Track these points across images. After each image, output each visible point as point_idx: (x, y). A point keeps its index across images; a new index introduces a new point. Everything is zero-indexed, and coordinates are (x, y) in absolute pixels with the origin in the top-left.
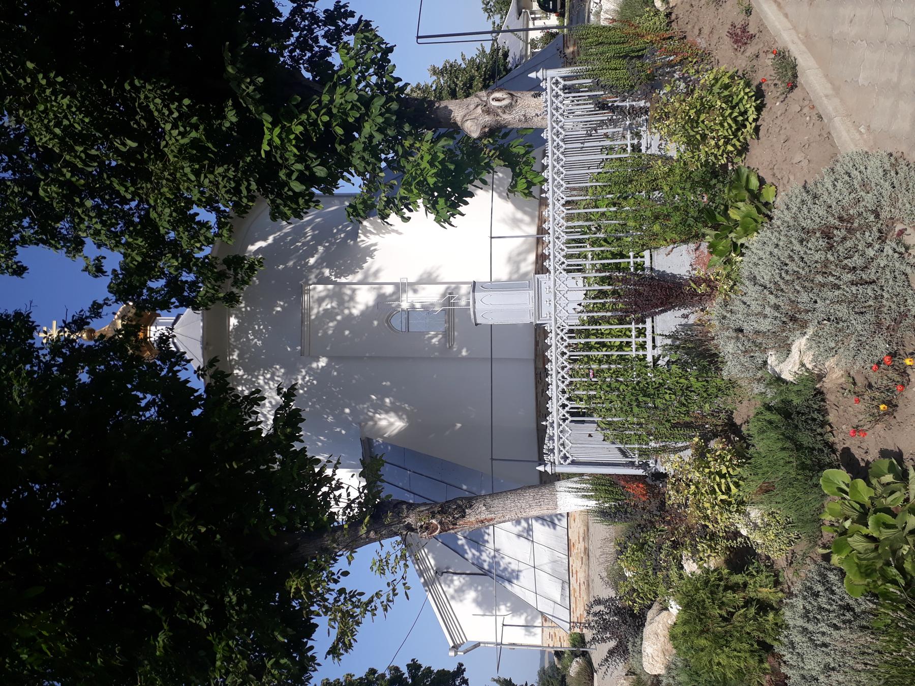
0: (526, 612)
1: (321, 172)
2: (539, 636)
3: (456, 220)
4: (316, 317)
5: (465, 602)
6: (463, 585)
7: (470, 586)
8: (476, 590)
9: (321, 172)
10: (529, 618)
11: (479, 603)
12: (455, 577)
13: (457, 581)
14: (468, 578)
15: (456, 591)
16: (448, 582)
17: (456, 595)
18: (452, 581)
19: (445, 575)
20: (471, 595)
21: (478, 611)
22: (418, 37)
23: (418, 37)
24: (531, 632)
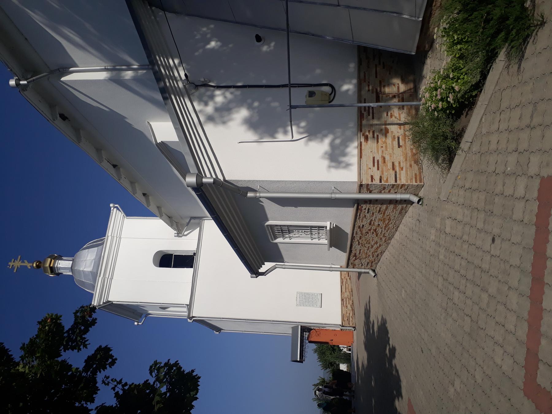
0: (334, 134)
1: (110, 360)
2: (355, 168)
3: (316, 404)
4: (69, 112)
5: (231, 124)
6: (230, 102)
7: (240, 103)
8: (250, 107)
9: (110, 360)
10: (338, 141)
11: (251, 124)
12: (218, 92)
13: (220, 97)
14: (238, 92)
15: (217, 109)
16: (205, 98)
17: (216, 115)
18: (212, 97)
19: (202, 90)
20: (243, 113)
21: (251, 136)
22: (292, 107)
23: (292, 107)
24: (340, 163)
